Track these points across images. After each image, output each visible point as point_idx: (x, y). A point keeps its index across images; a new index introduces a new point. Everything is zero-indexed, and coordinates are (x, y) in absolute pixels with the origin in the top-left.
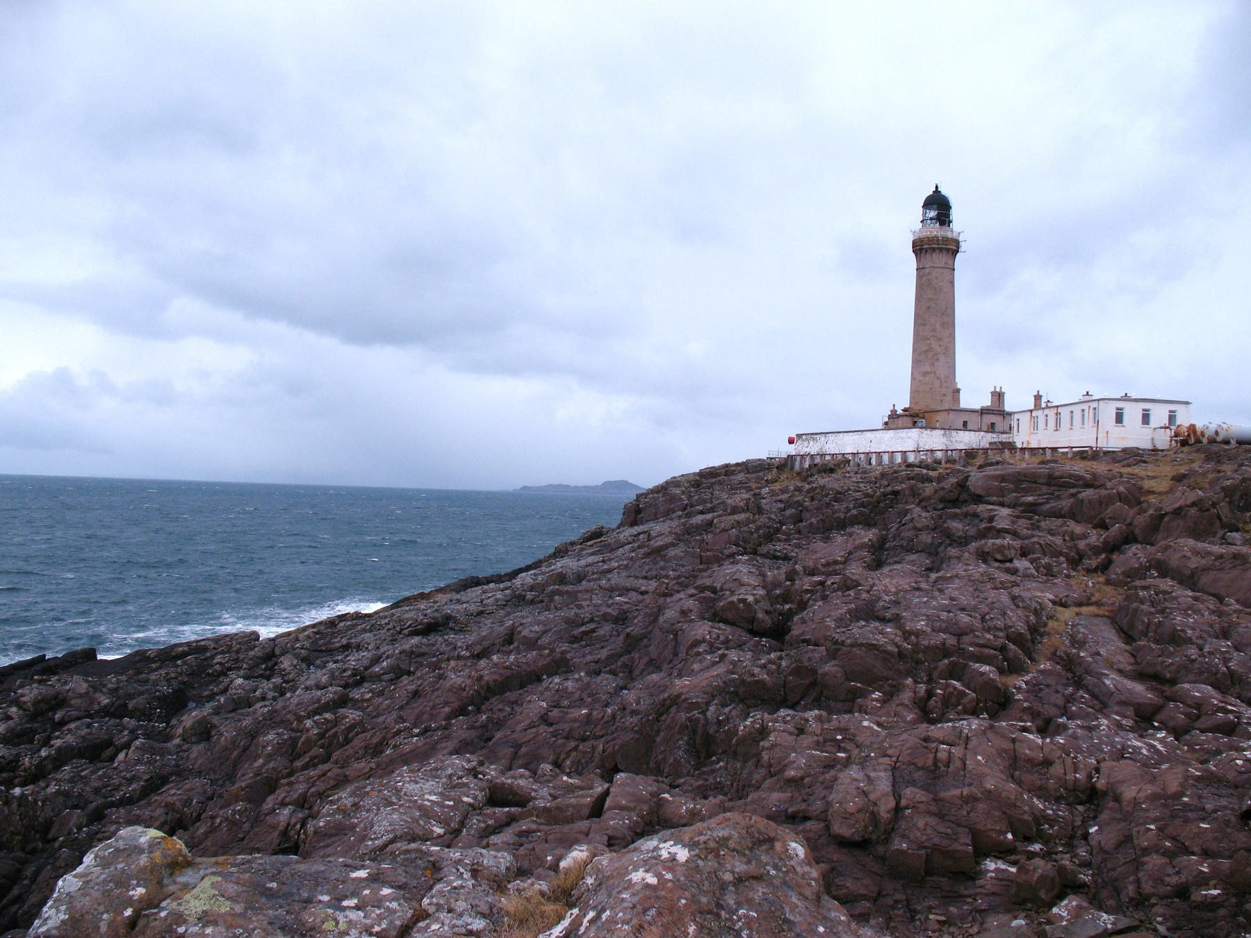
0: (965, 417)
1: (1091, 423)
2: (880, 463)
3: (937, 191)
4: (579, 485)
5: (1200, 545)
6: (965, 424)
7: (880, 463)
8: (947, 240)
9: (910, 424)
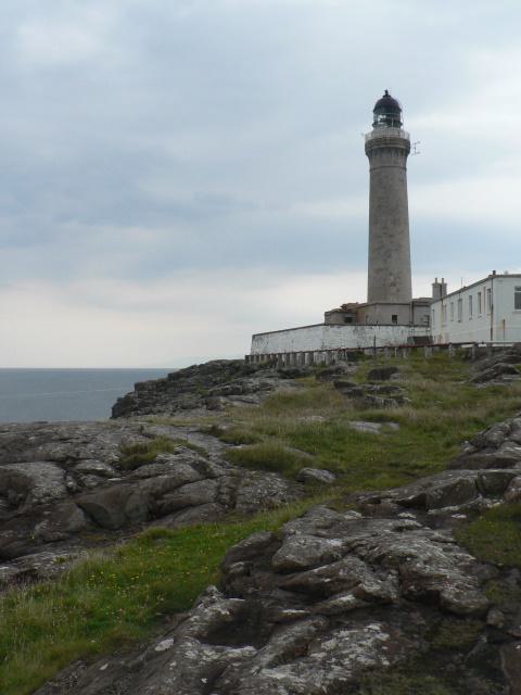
0: (395, 311)
1: (487, 307)
2: (311, 359)
3: (387, 95)
4: (144, 381)
5: (204, 460)
6: (394, 318)
7: (311, 359)
8: (394, 140)
9: (342, 321)
